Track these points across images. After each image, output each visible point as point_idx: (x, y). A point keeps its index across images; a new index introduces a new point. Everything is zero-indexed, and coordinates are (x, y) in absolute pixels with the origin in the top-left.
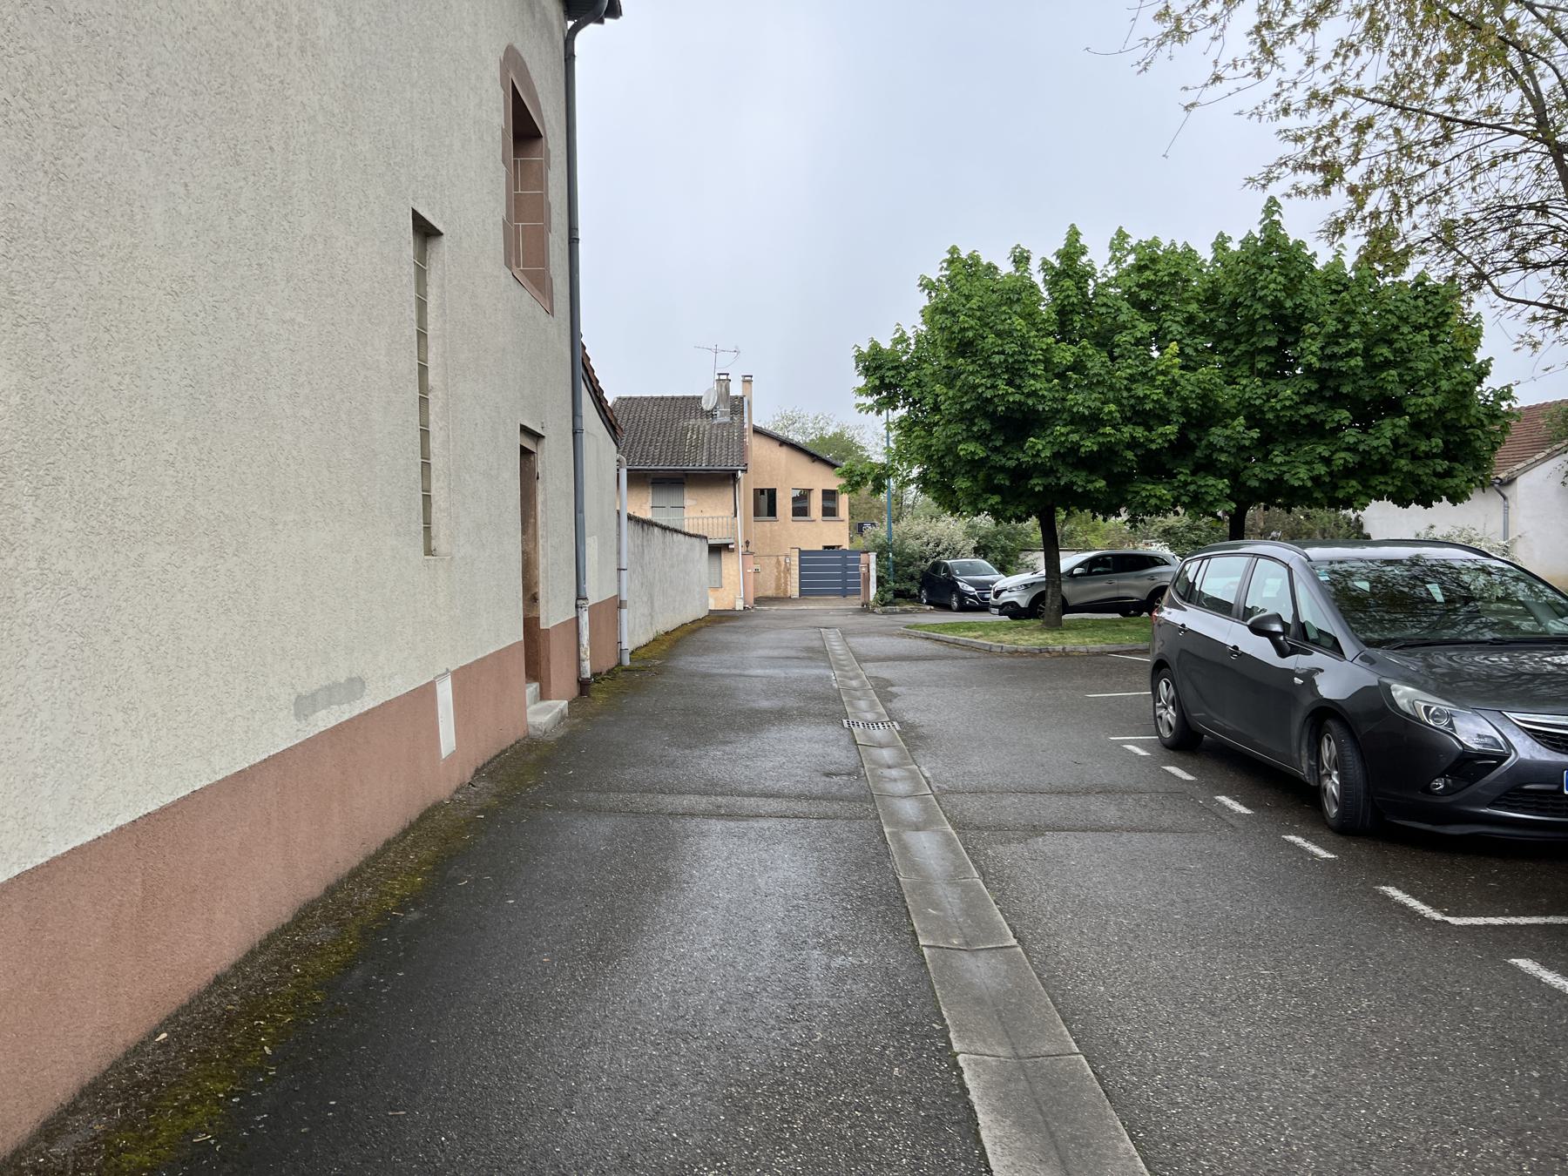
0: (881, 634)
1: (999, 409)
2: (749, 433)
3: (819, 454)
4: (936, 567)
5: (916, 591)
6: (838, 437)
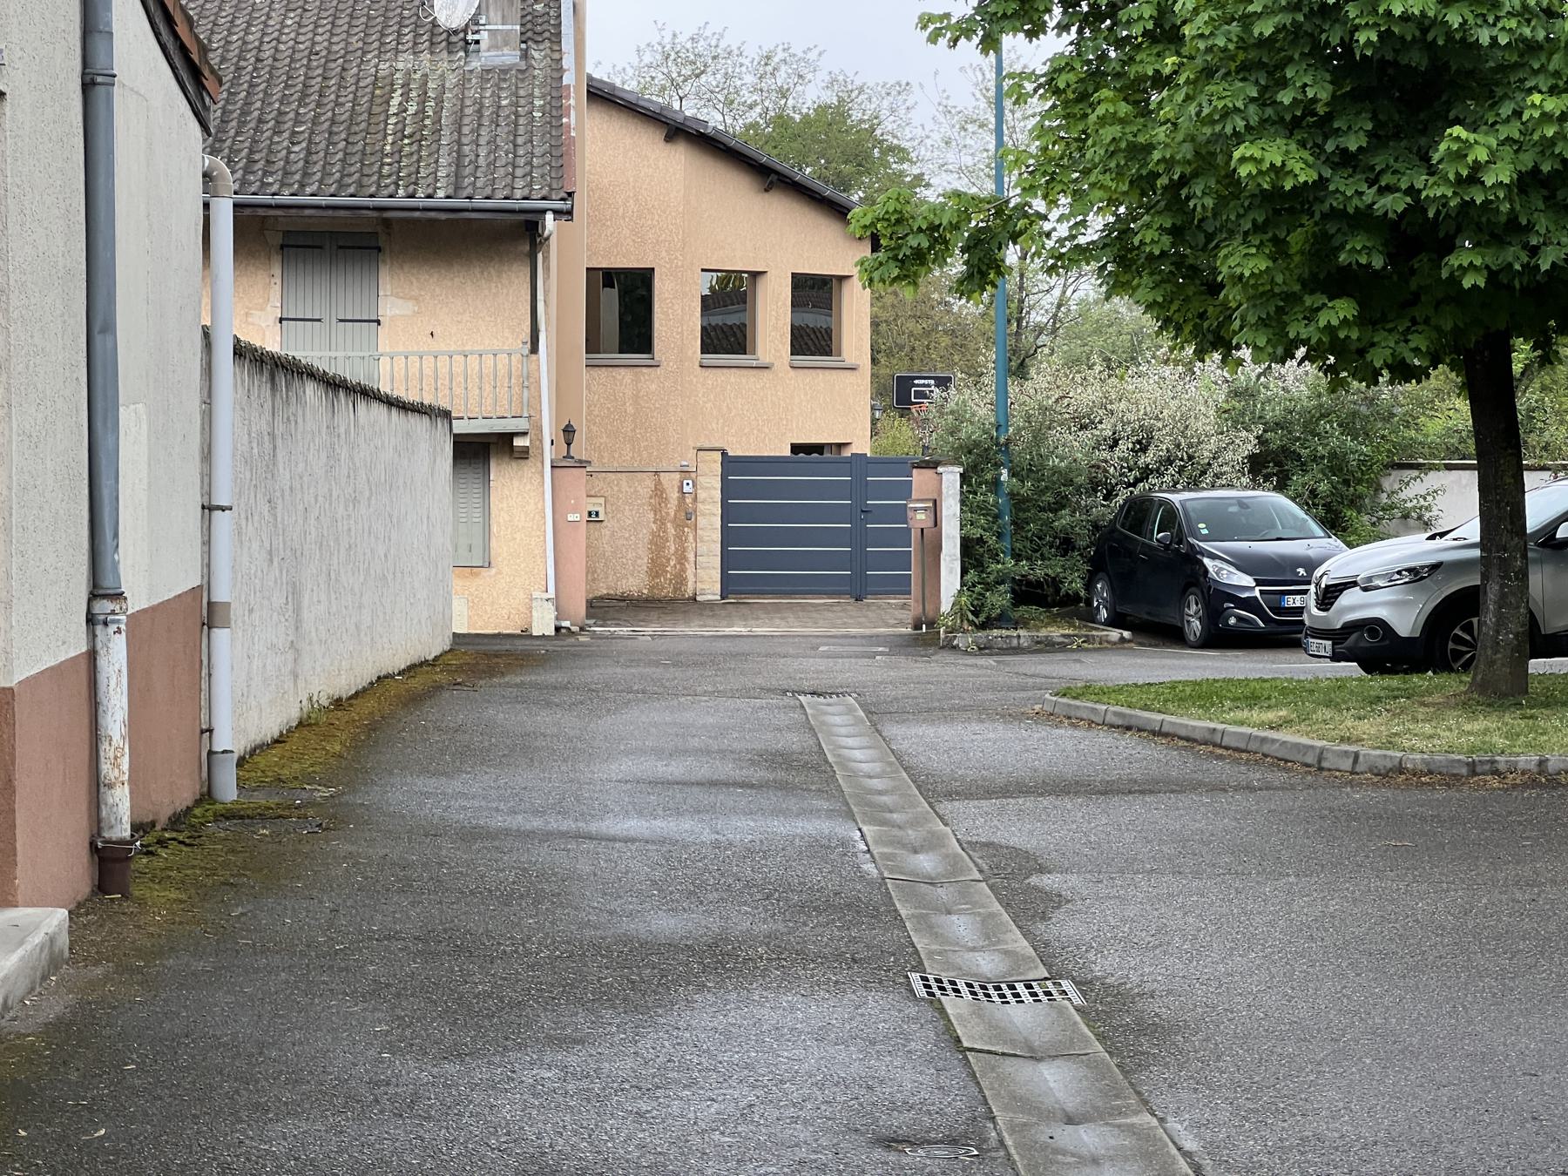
0: (983, 713)
1: (1362, 37)
2: (576, 99)
3: (784, 166)
4: (1139, 511)
5: (1078, 585)
6: (831, 119)
